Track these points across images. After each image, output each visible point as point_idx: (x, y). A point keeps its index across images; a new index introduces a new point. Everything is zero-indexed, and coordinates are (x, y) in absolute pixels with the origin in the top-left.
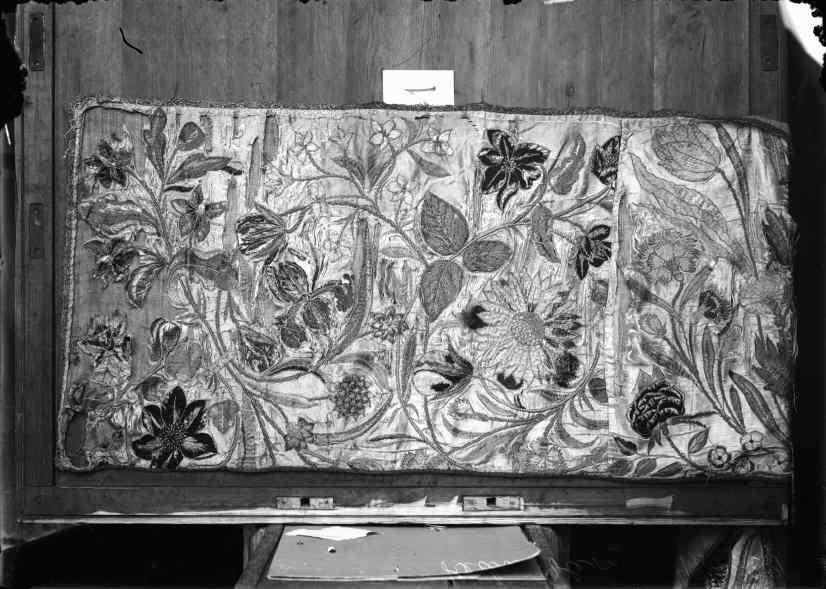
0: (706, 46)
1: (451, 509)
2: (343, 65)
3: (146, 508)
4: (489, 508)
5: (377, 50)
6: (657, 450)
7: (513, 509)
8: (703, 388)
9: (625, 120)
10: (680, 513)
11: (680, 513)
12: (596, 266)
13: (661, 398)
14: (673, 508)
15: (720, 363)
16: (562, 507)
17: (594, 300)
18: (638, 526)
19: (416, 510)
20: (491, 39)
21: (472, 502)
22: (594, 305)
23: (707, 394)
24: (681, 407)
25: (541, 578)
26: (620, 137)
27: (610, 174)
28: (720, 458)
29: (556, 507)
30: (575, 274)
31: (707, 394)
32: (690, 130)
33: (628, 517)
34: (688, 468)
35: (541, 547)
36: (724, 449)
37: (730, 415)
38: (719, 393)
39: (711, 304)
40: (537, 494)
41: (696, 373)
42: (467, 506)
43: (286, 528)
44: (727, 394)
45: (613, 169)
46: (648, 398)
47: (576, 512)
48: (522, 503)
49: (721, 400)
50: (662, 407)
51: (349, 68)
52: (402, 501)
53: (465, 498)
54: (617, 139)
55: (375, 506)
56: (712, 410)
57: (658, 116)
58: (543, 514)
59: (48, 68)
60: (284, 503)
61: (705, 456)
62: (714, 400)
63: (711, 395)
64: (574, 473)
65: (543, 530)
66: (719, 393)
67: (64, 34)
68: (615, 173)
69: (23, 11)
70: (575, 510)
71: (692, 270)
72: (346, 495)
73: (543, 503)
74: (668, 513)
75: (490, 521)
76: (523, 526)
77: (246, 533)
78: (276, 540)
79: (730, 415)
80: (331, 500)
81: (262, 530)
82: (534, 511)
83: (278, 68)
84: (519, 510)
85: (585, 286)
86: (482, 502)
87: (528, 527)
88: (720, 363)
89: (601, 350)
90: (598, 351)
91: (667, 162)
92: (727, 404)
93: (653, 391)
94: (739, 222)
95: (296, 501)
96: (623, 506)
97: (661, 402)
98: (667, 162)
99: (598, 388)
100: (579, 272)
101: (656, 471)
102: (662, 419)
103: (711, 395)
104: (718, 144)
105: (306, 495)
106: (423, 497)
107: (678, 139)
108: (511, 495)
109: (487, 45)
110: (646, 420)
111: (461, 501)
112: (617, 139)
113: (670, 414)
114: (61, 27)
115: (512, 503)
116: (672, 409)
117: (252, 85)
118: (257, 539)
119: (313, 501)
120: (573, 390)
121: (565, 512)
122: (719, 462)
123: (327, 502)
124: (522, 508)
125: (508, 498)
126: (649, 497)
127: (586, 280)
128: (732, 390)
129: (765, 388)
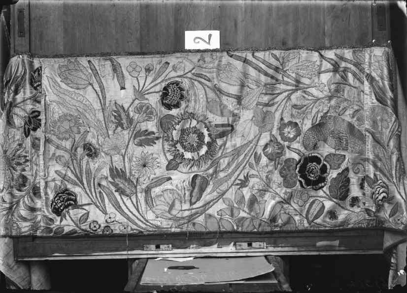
0: (351, 20)
1: (230, 249)
2: (172, 31)
3: (80, 252)
4: (249, 248)
5: (189, 24)
6: (64, 222)
7: (261, 248)
8: (86, 191)
9: (41, 59)
10: (342, 248)
11: (342, 248)
12: (34, 131)
13: (65, 196)
14: (339, 246)
15: (94, 179)
16: (285, 247)
17: (34, 148)
18: (322, 255)
19: (213, 249)
20: (245, 17)
21: (240, 245)
22: (33, 151)
23: (88, 195)
24: (75, 201)
25: (275, 282)
26: (41, 67)
27: (38, 86)
28: (95, 227)
29: (282, 247)
30: (23, 135)
31: (88, 195)
32: (75, 64)
33: (317, 251)
34: (80, 231)
35: (274, 266)
36: (97, 222)
37: (99, 205)
38: (94, 194)
39: (90, 150)
40: (272, 240)
41: (83, 184)
42: (238, 247)
43: (149, 260)
44: (98, 195)
45: (39, 83)
46: (60, 197)
47: (291, 249)
48: (265, 245)
49: (95, 198)
50: (67, 201)
51: (176, 32)
52: (205, 245)
53: (237, 243)
54: (40, 68)
55: (193, 248)
56: (92, 203)
57: (58, 57)
58: (275, 250)
59: (27, 35)
60: (147, 248)
61: (88, 226)
62: (92, 198)
63: (90, 195)
64: (26, 234)
65: (275, 258)
66: (94, 194)
67: (34, 19)
68: (41, 85)
69: (14, 8)
70: (291, 248)
71: (79, 132)
72: (177, 243)
73: (275, 245)
74: (337, 248)
75: (249, 254)
76: (266, 257)
77: (129, 262)
78: (144, 265)
79: (99, 205)
80: (171, 246)
81: (137, 261)
82: (271, 249)
83: (141, 34)
84: (263, 248)
85: (28, 141)
86: (245, 245)
87: (268, 257)
88: (94, 179)
89: (38, 173)
90: (36, 173)
91: (65, 79)
92: (98, 200)
93: (61, 193)
94: (101, 110)
95: (153, 247)
96: (314, 246)
97: (66, 198)
98: (65, 80)
99: (36, 191)
100: (25, 134)
101: (64, 233)
102: (66, 207)
103: (90, 195)
104: (90, 71)
105: (158, 243)
106: (216, 243)
107: (70, 68)
108: (259, 241)
109: (243, 21)
110: (59, 208)
111: (235, 245)
112: (40, 68)
113: (70, 205)
114: (33, 16)
115: (260, 245)
116: (71, 202)
117: (128, 42)
118: (134, 265)
119: (161, 246)
120: (24, 193)
121: (286, 249)
122: (95, 229)
123: (168, 247)
124: (265, 247)
125: (258, 243)
126: (328, 241)
127: (29, 138)
128: (100, 192)
129: (115, 191)
